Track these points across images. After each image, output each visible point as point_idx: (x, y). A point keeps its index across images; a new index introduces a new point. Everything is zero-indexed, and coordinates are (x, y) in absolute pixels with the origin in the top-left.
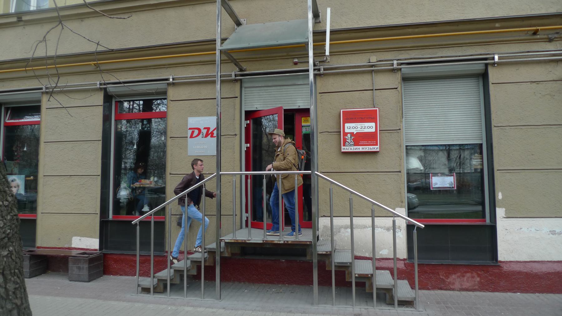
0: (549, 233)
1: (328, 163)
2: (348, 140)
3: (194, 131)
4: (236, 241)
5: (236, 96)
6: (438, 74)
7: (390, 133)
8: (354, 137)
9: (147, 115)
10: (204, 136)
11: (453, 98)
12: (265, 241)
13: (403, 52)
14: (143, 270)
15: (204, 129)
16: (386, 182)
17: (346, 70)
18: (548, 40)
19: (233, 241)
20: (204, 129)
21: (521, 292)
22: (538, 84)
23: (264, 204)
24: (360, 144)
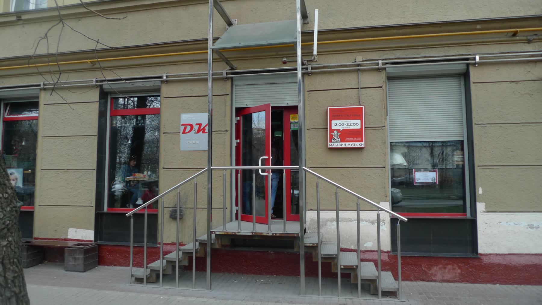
0: (527, 226)
2: (334, 136)
4: (226, 233)
5: (227, 94)
9: (141, 111)
10: (196, 132)
12: (254, 234)
13: (388, 52)
15: (196, 125)
16: (371, 177)
18: (527, 41)
20: (196, 125)
24: (346, 140)
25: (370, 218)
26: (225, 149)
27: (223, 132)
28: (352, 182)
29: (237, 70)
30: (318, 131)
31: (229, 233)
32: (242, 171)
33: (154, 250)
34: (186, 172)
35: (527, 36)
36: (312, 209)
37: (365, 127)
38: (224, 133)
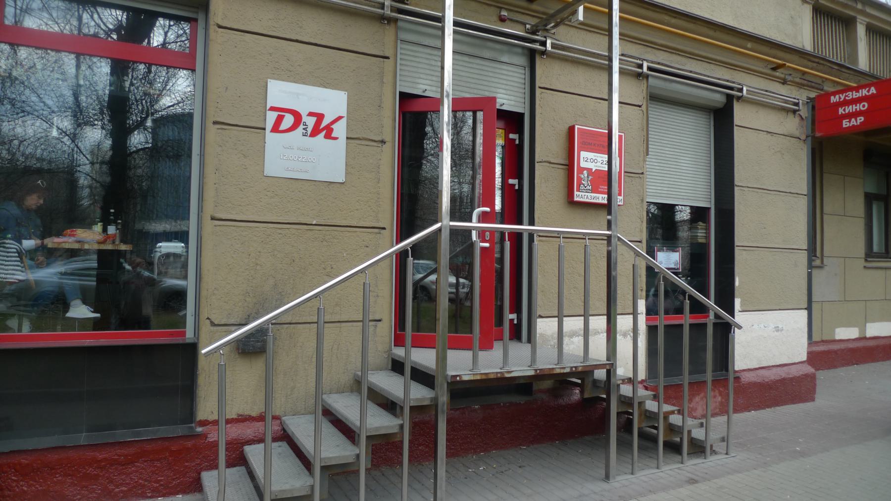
0: (774, 330)
1: (548, 218)
2: (583, 181)
3: (283, 116)
4: (484, 377)
5: (387, 55)
6: (686, 98)
7: (631, 178)
8: (592, 177)
9: (127, 50)
10: (309, 133)
11: (670, 134)
12: (538, 371)
13: (649, 49)
14: (127, 484)
15: (308, 115)
16: (624, 257)
17: (578, 56)
18: (782, 81)
19: (478, 377)
20: (308, 115)
21: (755, 410)
22: (772, 135)
23: (661, 296)
24: (599, 190)
25: (622, 327)
26: (378, 183)
27: (375, 144)
28: (599, 265)
29: (410, 6)
30: (553, 168)
31: (489, 375)
32: (480, 232)
33: (189, 444)
34: (280, 231)
35: (786, 75)
36: (542, 315)
37: (625, 172)
38: (379, 145)
